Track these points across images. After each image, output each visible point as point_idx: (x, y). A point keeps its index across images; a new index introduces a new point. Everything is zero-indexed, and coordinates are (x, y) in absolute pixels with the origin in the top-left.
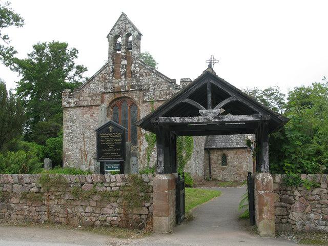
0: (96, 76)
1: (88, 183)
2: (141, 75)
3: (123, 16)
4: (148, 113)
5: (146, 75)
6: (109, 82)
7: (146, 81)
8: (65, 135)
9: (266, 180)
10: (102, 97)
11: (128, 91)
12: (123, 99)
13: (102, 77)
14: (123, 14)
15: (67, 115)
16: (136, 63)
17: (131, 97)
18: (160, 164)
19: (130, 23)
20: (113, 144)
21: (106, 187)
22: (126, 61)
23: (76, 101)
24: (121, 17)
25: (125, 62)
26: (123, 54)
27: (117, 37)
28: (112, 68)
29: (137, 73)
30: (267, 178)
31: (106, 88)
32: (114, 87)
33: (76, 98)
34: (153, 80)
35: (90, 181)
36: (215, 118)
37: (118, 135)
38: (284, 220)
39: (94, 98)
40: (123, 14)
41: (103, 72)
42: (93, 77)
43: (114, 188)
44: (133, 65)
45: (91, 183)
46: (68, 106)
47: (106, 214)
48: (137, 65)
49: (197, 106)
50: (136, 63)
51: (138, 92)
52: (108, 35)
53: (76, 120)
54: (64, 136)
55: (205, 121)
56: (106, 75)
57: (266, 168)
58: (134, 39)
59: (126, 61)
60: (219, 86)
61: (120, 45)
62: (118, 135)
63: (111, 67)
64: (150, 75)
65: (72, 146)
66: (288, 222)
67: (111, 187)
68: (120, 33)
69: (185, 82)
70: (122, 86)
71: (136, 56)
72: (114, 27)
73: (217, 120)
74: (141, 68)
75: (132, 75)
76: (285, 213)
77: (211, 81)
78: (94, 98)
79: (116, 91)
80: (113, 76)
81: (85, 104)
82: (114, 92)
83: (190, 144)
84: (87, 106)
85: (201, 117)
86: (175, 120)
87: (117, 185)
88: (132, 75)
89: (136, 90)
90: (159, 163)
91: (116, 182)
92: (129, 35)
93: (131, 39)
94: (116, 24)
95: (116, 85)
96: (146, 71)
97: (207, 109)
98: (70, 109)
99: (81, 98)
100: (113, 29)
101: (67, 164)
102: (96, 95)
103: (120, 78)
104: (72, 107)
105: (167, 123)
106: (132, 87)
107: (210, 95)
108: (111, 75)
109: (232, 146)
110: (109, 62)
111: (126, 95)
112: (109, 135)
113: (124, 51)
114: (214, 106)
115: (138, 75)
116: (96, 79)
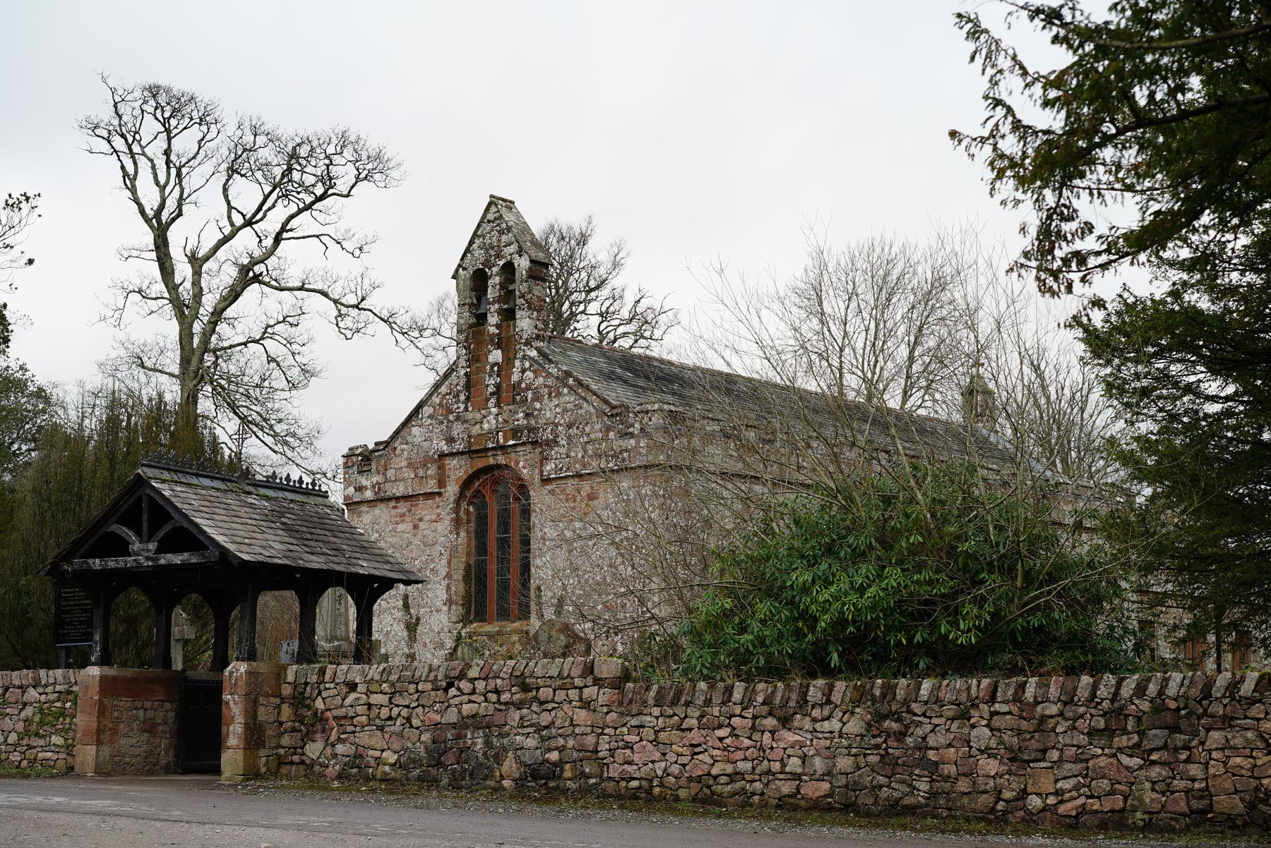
2: (537, 398)
5: (550, 394)
6: (458, 418)
7: (548, 415)
10: (441, 468)
11: (503, 448)
13: (440, 405)
21: (40, 694)
22: (499, 352)
24: (487, 209)
25: (496, 356)
28: (466, 374)
29: (528, 388)
31: (450, 440)
33: (378, 473)
36: (148, 558)
39: (421, 473)
41: (443, 389)
44: (517, 363)
48: (527, 364)
49: (127, 538)
51: (529, 447)
52: (457, 271)
55: (135, 564)
59: (499, 352)
63: (462, 372)
66: (303, 762)
69: (647, 412)
70: (490, 432)
71: (525, 336)
72: (471, 243)
73: (150, 563)
75: (514, 396)
76: (300, 743)
79: (473, 448)
80: (468, 399)
81: (399, 490)
82: (469, 453)
84: (406, 498)
89: (523, 444)
94: (475, 235)
95: (476, 430)
96: (550, 382)
98: (364, 508)
99: (390, 473)
100: (467, 251)
104: (369, 502)
106: (515, 432)
108: (462, 398)
111: (501, 460)
116: (427, 410)
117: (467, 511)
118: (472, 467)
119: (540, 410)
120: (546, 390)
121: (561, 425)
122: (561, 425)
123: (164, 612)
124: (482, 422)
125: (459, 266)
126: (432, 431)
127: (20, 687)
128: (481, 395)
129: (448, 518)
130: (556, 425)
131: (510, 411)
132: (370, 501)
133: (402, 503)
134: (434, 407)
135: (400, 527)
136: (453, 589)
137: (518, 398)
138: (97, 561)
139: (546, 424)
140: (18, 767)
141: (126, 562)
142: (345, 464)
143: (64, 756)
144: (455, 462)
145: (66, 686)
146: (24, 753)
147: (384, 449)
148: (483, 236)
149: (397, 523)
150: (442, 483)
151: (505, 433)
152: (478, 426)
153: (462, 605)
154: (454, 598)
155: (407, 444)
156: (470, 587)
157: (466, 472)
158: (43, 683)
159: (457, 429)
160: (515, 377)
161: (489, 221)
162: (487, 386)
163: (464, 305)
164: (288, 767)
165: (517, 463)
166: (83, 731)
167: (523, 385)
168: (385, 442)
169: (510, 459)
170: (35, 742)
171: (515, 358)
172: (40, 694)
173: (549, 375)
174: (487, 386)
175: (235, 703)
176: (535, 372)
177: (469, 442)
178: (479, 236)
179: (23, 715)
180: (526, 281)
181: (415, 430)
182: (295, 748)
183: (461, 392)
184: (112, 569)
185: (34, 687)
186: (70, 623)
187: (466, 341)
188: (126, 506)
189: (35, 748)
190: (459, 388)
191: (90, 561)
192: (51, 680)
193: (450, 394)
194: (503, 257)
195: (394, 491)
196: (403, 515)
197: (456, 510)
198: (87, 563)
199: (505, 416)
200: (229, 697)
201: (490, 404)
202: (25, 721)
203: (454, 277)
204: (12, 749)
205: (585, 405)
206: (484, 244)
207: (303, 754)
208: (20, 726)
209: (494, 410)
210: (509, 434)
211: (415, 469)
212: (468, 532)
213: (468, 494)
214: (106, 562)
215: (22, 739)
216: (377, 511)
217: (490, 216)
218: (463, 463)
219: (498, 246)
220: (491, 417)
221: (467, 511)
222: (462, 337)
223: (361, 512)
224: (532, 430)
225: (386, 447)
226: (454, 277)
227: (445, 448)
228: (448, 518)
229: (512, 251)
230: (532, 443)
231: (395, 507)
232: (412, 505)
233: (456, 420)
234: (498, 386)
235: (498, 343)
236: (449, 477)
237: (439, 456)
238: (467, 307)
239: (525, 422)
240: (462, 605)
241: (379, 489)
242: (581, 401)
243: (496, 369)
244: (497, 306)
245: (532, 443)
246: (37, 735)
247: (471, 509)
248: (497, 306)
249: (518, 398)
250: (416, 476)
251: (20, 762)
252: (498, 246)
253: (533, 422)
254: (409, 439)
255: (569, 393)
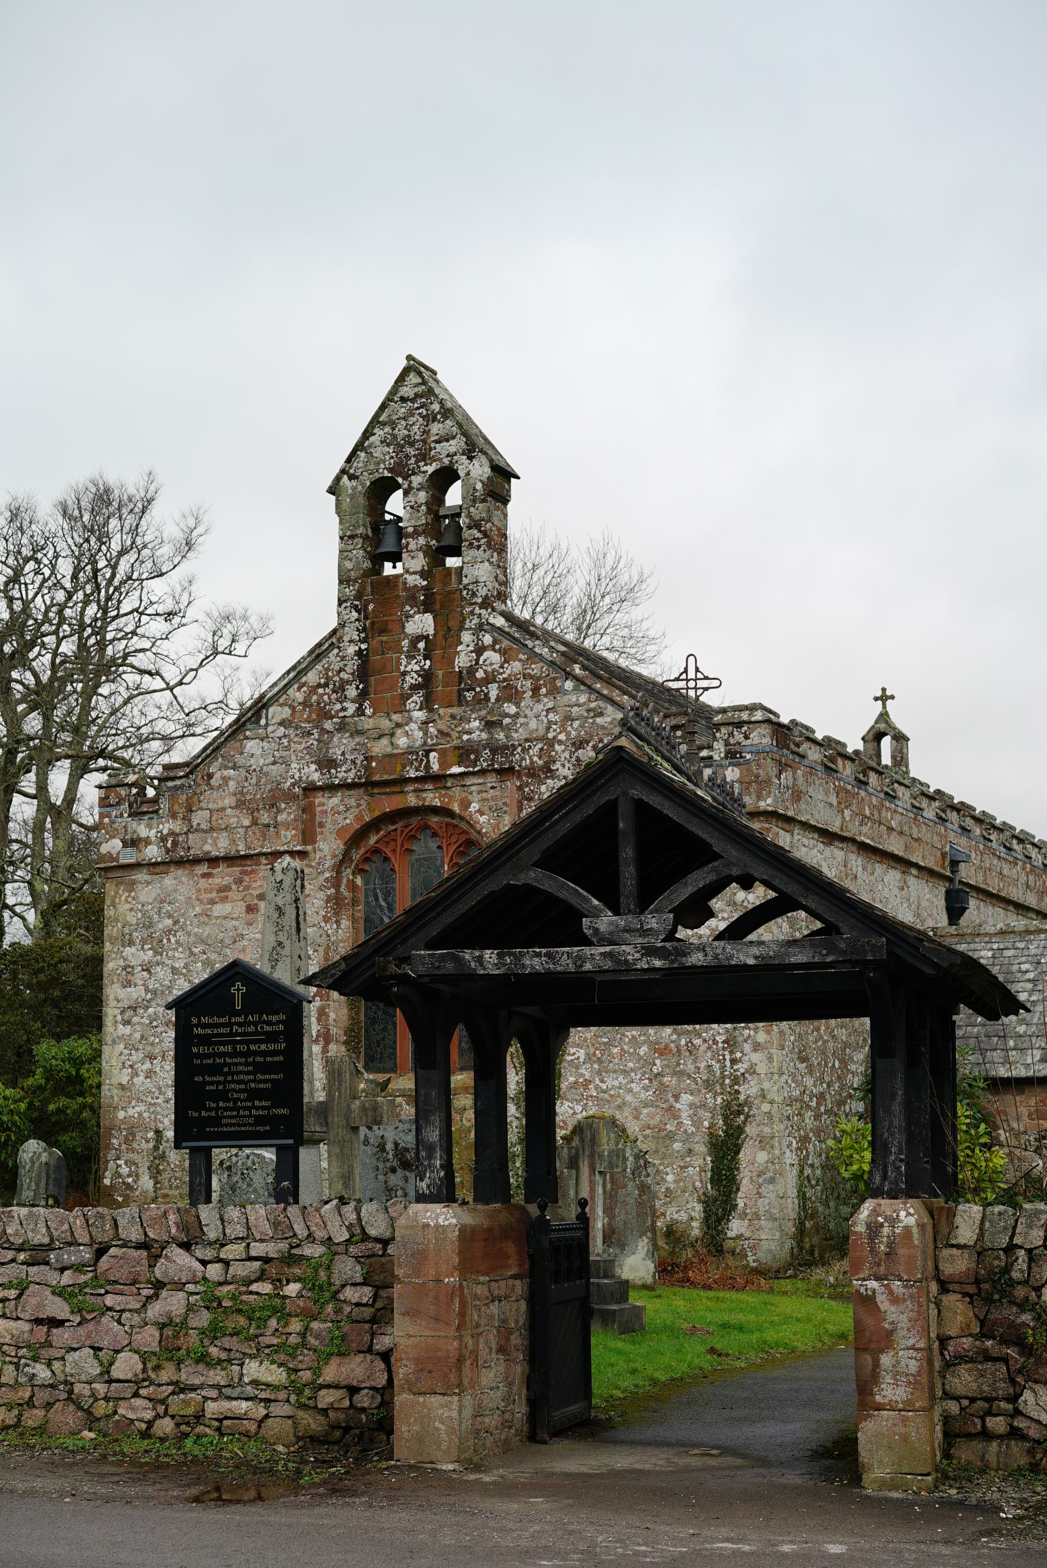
0: (274, 698)
1: (125, 1245)
2: (510, 693)
3: (413, 379)
4: (206, 976)
5: (536, 690)
6: (342, 727)
7: (533, 724)
8: (111, 1012)
9: (886, 1230)
10: (308, 810)
11: (438, 780)
12: (415, 821)
13: (305, 704)
14: (413, 367)
15: (123, 908)
16: (480, 628)
17: (456, 808)
18: (430, 1157)
19: (447, 412)
20: (247, 1064)
21: (204, 1263)
22: (429, 618)
23: (172, 833)
24: (401, 379)
25: (423, 623)
26: (414, 580)
27: (382, 489)
28: (359, 653)
29: (489, 679)
30: (893, 1221)
31: (327, 764)
32: (368, 759)
33: (174, 816)
34: (569, 718)
35: (135, 1235)
36: (649, 951)
37: (270, 1023)
38: (997, 1424)
39: (265, 818)
40: (413, 367)
41: (312, 677)
42: (260, 706)
43: (239, 1270)
44: (466, 637)
45: (139, 1246)
46: (129, 857)
47: (201, 1387)
48: (488, 639)
49: (574, 901)
50: (480, 628)
51: (491, 779)
52: (338, 479)
53: (169, 931)
54: (108, 1021)
55: (608, 965)
56: (325, 694)
57: (891, 1174)
58: (471, 497)
59: (429, 618)
60: (670, 810)
61: (400, 533)
62: (270, 1023)
63: (352, 649)
64: (554, 691)
65: (149, 1074)
66: (1015, 1433)
67: (227, 1263)
68: (401, 469)
69: (739, 725)
70: (410, 751)
71: (483, 592)
72: (367, 433)
73: (658, 963)
74: (507, 656)
75: (460, 693)
76: (1004, 1388)
77: (636, 793)
78: (265, 818)
79: (377, 778)
80: (363, 695)
81: (220, 845)
82: (367, 785)
83: (410, 1079)
84: (230, 859)
85: (588, 951)
86: (480, 960)
87: (253, 1253)
88: (460, 693)
89: (483, 772)
90: (423, 1154)
91: (247, 1238)
92: (446, 477)
93: (454, 496)
94: (375, 421)
95: (380, 747)
96: (536, 669)
97: (617, 913)
98: (141, 876)
99: (199, 818)
100: (359, 447)
101: (125, 1170)
102: (275, 799)
103: (401, 709)
104: (153, 866)
105: (445, 979)
106: (465, 753)
107: (627, 853)
108: (352, 692)
109: (1021, 1072)
110: (342, 625)
111: (432, 798)
112: (230, 1025)
113: (419, 562)
114: (644, 904)
115: (494, 691)
116: (277, 713)
117: (352, 886)
118: (370, 808)
119: (516, 716)
120: (528, 683)
121: (560, 742)
122: (560, 742)
123: (461, 1079)
124: (392, 735)
125: (343, 471)
126: (288, 748)
127: (144, 1245)
128: (392, 687)
129: (321, 895)
130: (551, 743)
131: (453, 717)
132: (156, 864)
133: (222, 867)
134: (293, 708)
135: (218, 909)
136: (332, 1015)
137: (469, 695)
138: (490, 956)
139: (527, 740)
140: (145, 1435)
141: (580, 959)
142: (101, 799)
143: (287, 1410)
144: (335, 800)
145: (283, 1246)
146: (163, 1401)
147: (186, 776)
148: (393, 424)
149: (212, 902)
150: (308, 835)
151: (443, 754)
152: (385, 741)
153: (345, 1043)
154: (334, 1031)
155: (234, 768)
156: (357, 1013)
157: (358, 818)
158: (212, 1235)
159: (341, 746)
160: (463, 660)
161: (403, 399)
162: (404, 674)
163: (352, 537)
164: (977, 1445)
165: (466, 804)
166: (417, 1361)
167: (480, 674)
168: (186, 764)
169: (451, 798)
170: (188, 1375)
171: (462, 628)
172: (204, 1263)
173: (534, 656)
174: (404, 674)
175: (895, 1300)
176: (503, 652)
177: (367, 768)
178: (384, 424)
179: (155, 1311)
180: (484, 501)
181: (251, 746)
182: (990, 1400)
183: (349, 683)
184: (535, 976)
185: (186, 1246)
186: (222, 1095)
187: (359, 596)
188: (566, 826)
189: (193, 1389)
190: (343, 675)
191: (467, 955)
192: (236, 1230)
193: (326, 685)
194: (433, 459)
195: (207, 848)
196: (227, 888)
197: (336, 882)
198: (458, 960)
199: (442, 725)
200: (873, 1284)
201: (410, 705)
202: (162, 1327)
203: (332, 491)
204: (128, 1390)
205: (610, 709)
206: (395, 437)
207: (1018, 1412)
208: (149, 1338)
209: (419, 715)
210: (452, 757)
211: (253, 812)
212: (354, 920)
213: (357, 855)
214: (518, 958)
215: (157, 1368)
216: (168, 881)
217: (406, 391)
218: (352, 802)
219: (424, 441)
220: (413, 726)
221: (352, 886)
222: (350, 591)
223: (133, 883)
224: (496, 749)
225: (191, 772)
226: (332, 491)
227: (316, 776)
228: (321, 895)
229: (453, 450)
230: (499, 772)
231: (205, 875)
232: (245, 873)
233: (338, 730)
234: (427, 676)
235: (424, 603)
236: (321, 825)
237: (305, 789)
238: (359, 541)
239: (484, 736)
240: (345, 1043)
241: (175, 844)
242: (601, 704)
243: (421, 645)
244: (422, 541)
245: (499, 772)
246: (203, 1359)
247: (359, 881)
248: (422, 541)
249: (469, 695)
250: (255, 822)
251: (150, 1424)
252: (424, 441)
253: (502, 736)
254: (240, 760)
255: (576, 689)
